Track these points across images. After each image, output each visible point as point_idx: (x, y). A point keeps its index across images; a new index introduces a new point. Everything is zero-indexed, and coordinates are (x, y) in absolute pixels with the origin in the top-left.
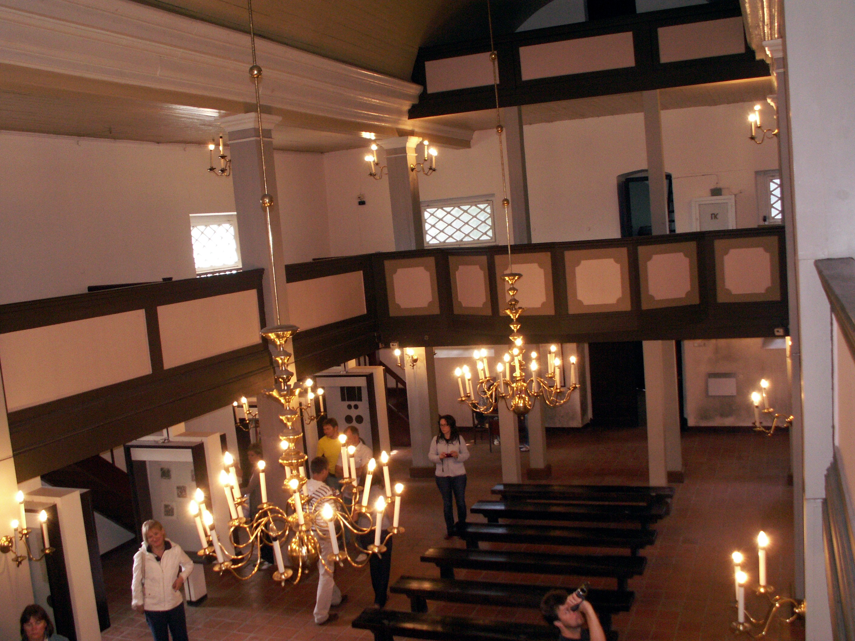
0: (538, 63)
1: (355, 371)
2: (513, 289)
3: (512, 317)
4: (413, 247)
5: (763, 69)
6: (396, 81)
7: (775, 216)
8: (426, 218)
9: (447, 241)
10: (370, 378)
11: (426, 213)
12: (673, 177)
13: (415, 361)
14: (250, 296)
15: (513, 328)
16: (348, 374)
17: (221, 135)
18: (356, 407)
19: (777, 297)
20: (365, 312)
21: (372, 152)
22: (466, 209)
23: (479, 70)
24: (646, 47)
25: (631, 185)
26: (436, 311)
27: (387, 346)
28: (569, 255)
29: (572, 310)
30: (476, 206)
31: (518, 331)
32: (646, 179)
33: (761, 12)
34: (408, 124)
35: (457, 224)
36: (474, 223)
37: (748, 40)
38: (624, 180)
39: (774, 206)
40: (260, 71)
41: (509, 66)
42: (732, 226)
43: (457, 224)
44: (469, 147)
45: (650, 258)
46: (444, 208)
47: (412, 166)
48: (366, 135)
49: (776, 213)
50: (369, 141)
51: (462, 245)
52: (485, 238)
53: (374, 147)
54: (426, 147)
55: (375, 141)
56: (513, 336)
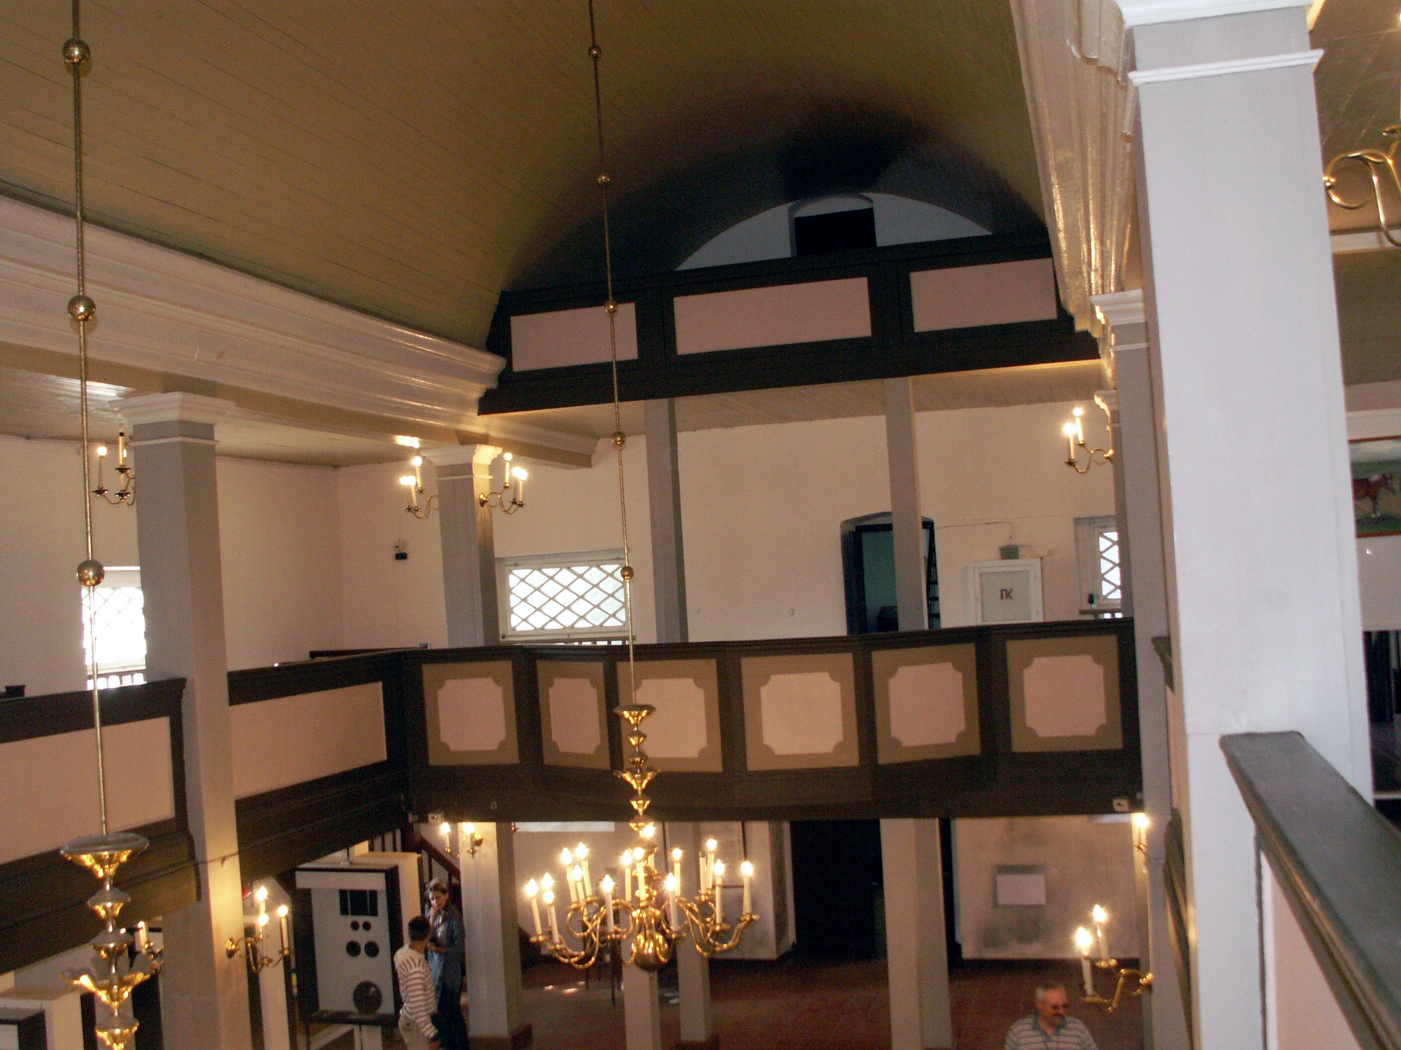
0: (705, 324)
1: (366, 860)
2: (639, 734)
3: (635, 787)
4: (478, 641)
5: (1087, 347)
6: (457, 347)
7: (1108, 594)
8: (511, 586)
9: (546, 628)
10: (392, 876)
11: (511, 576)
12: (936, 525)
13: (478, 843)
14: (158, 729)
15: (635, 806)
16: (353, 867)
17: (121, 431)
18: (367, 926)
19: (1116, 742)
20: (384, 756)
21: (412, 471)
22: (581, 573)
23: (604, 333)
24: (891, 304)
25: (866, 537)
26: (512, 757)
27: (424, 819)
28: (749, 665)
29: (755, 763)
30: (598, 567)
31: (645, 812)
32: (888, 527)
33: (1085, 247)
34: (478, 424)
35: (566, 598)
36: (595, 596)
37: (1062, 299)
38: (853, 529)
39: (1106, 576)
40: (91, 306)
41: (656, 328)
42: (1036, 617)
43: (566, 598)
44: (589, 466)
45: (893, 672)
46: (543, 570)
47: (482, 496)
48: (403, 440)
49: (1111, 587)
50: (408, 452)
51: (573, 634)
52: (612, 623)
53: (417, 462)
54: (508, 464)
55: (418, 452)
56: (637, 821)
